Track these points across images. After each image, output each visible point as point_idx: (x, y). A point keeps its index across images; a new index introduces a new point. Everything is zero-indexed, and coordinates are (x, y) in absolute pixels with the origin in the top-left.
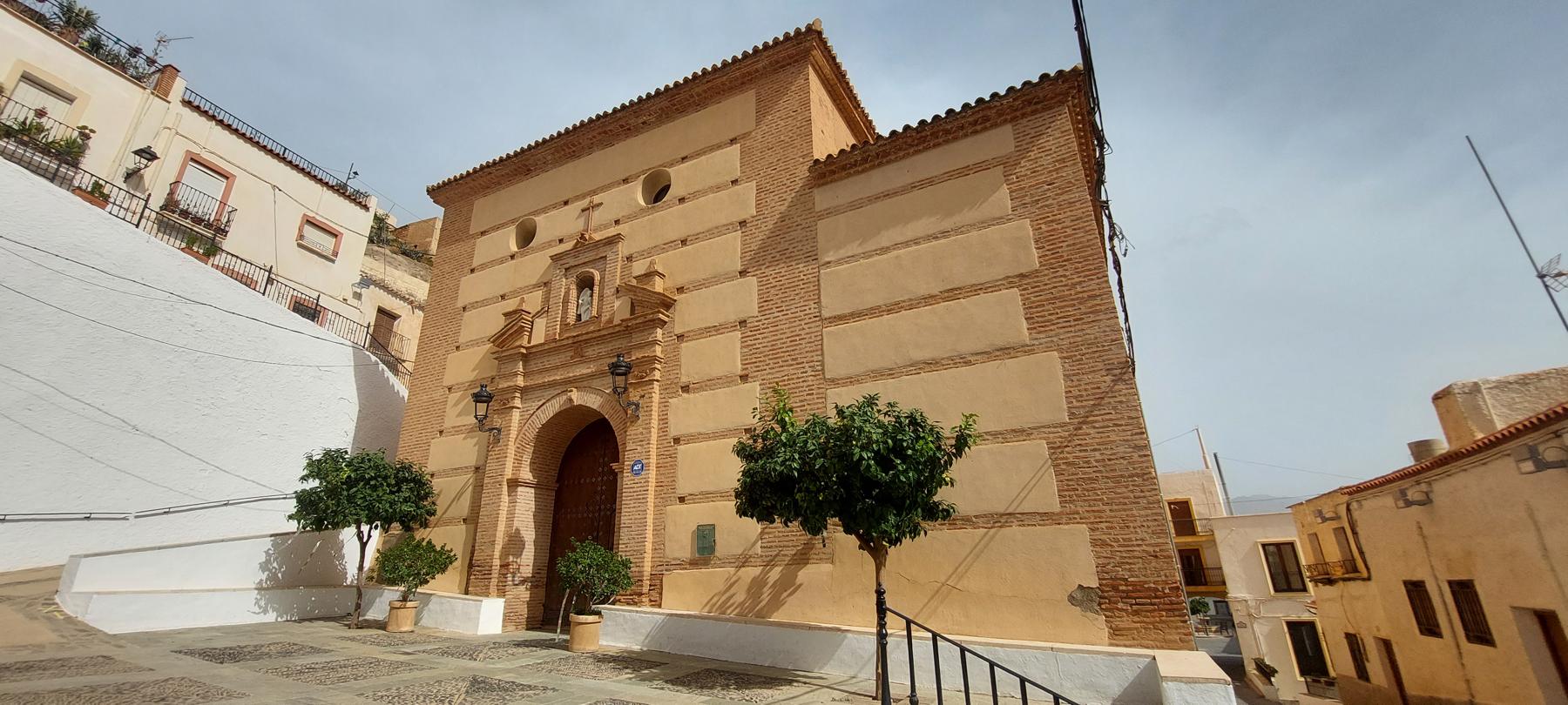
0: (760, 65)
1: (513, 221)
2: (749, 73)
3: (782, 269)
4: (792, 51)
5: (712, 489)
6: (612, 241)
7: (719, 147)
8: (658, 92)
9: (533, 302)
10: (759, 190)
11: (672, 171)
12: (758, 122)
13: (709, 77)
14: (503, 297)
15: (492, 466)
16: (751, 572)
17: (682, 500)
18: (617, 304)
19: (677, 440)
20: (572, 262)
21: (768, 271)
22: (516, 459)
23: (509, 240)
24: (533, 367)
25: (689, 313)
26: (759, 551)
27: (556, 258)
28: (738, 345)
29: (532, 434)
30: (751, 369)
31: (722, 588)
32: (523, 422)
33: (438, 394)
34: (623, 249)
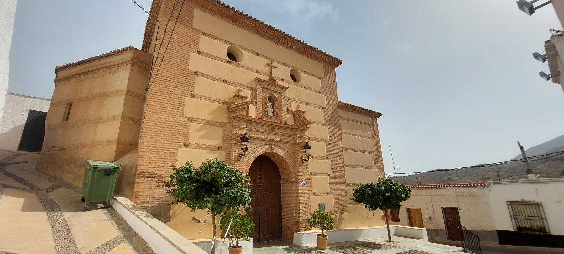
1: (227, 42)
7: (315, 76)
9: (246, 93)
11: (302, 74)
12: (325, 76)
14: (225, 82)
17: (314, 194)
18: (288, 116)
19: (311, 174)
20: (266, 86)
27: (257, 79)
33: (180, 119)
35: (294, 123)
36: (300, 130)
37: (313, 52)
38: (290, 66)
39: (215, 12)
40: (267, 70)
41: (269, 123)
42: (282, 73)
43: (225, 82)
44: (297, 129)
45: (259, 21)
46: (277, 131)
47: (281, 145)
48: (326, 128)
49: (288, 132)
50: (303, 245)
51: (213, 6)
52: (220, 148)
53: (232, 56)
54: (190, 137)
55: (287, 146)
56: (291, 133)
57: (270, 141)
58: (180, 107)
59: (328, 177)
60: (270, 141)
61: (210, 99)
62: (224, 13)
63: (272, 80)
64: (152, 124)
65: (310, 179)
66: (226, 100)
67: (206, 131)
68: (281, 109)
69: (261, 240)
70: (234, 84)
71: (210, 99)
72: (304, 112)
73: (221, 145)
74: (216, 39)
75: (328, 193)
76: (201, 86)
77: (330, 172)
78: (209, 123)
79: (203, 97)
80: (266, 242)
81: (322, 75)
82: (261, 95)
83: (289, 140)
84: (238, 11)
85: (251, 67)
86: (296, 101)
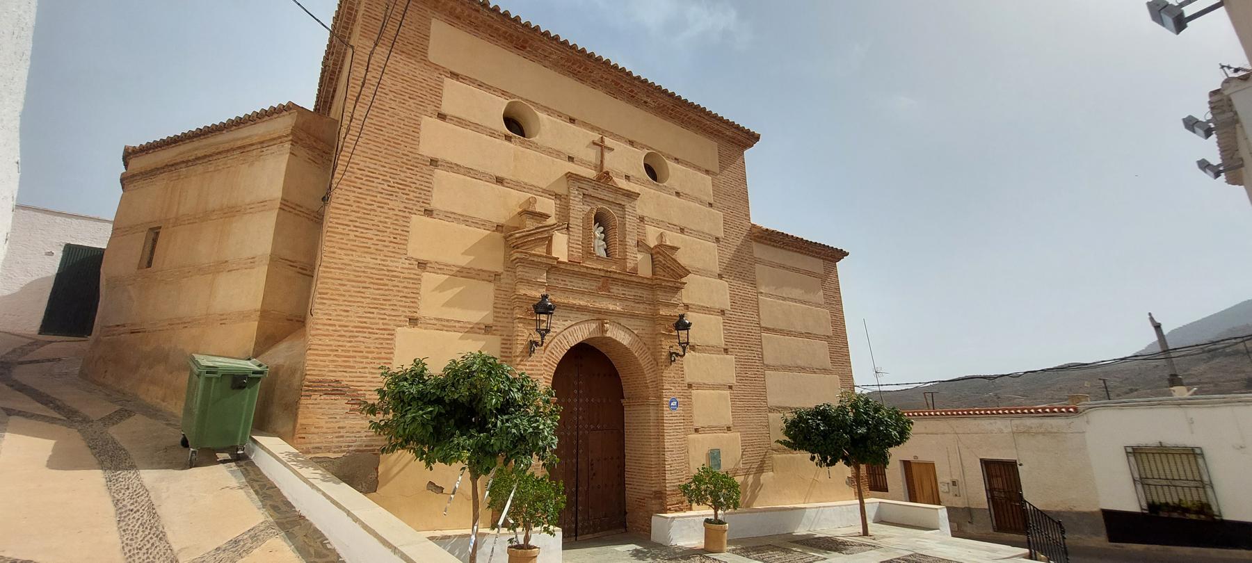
1: (504, 93)
7: (699, 169)
9: (547, 205)
11: (671, 164)
12: (722, 168)
14: (500, 181)
17: (696, 430)
18: (640, 256)
19: (690, 386)
20: (591, 191)
27: (569, 176)
33: (400, 264)
35: (654, 273)
36: (665, 287)
37: (694, 116)
38: (643, 147)
39: (477, 27)
40: (592, 155)
41: (597, 273)
42: (625, 162)
43: (500, 181)
44: (660, 286)
45: (574, 47)
46: (616, 290)
47: (623, 321)
48: (724, 284)
49: (639, 292)
50: (673, 543)
51: (474, 14)
52: (488, 329)
53: (515, 124)
54: (421, 305)
55: (638, 323)
56: (645, 294)
57: (600, 313)
58: (400, 238)
59: (728, 392)
60: (600, 313)
61: (467, 220)
62: (497, 29)
63: (604, 177)
64: (337, 274)
65: (689, 397)
66: (502, 221)
67: (457, 290)
68: (623, 242)
69: (579, 531)
70: (519, 186)
71: (467, 220)
72: (675, 249)
73: (490, 321)
74: (480, 86)
75: (729, 429)
76: (447, 190)
77: (733, 381)
78: (465, 273)
79: (450, 216)
80: (589, 536)
81: (715, 167)
82: (580, 210)
83: (640, 309)
84: (527, 25)
85: (558, 148)
86: (657, 223)
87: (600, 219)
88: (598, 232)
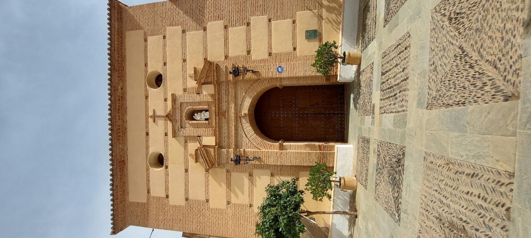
0: (117, 26)
1: (148, 170)
2: (118, 32)
3: (207, 11)
4: (116, 11)
5: (291, 34)
6: (174, 99)
7: (146, 47)
8: (110, 75)
9: (193, 146)
10: (171, 25)
11: (150, 70)
12: (141, 28)
13: (113, 49)
14: (186, 171)
15: (271, 161)
16: (325, 14)
17: (295, 49)
18: (205, 93)
19: (270, 54)
20: (179, 124)
21: (207, 17)
22: (270, 150)
23: (157, 172)
24: (225, 144)
25: (216, 55)
26: (316, 11)
27: (174, 135)
28: (234, 28)
29: (259, 139)
30: (245, 21)
31: (330, 25)
32: (251, 142)
33: (230, 212)
34: (179, 93)
35: (210, 83)
36: (218, 77)
37: (116, 55)
38: (146, 90)
39: (124, 183)
40: (161, 122)
41: (217, 120)
42: (158, 101)
43: (186, 171)
44: (218, 79)
45: (111, 140)
46: (224, 108)
47: (239, 102)
48: (209, 25)
49: (223, 92)
50: (353, 76)
51: (119, 187)
52: (251, 175)
53: (160, 161)
54: (244, 203)
55: (239, 92)
56: (224, 88)
57: (237, 117)
58: (220, 211)
59: (273, 22)
60: (237, 117)
61: (207, 186)
62: (121, 175)
63: (168, 117)
64: (237, 233)
65: (276, 55)
66: (204, 170)
67: (236, 189)
68: (200, 103)
69: (343, 112)
70: (186, 162)
71: (207, 186)
72: (195, 69)
73: (247, 174)
74: (148, 180)
75: (294, 22)
76: (197, 193)
77: (265, 17)
78: (229, 185)
79: (207, 192)
80: (345, 106)
81: (141, 32)
82: (189, 130)
83: (232, 91)
84: (112, 165)
85: (163, 142)
86: (185, 83)
87: (191, 116)
88: (197, 116)
